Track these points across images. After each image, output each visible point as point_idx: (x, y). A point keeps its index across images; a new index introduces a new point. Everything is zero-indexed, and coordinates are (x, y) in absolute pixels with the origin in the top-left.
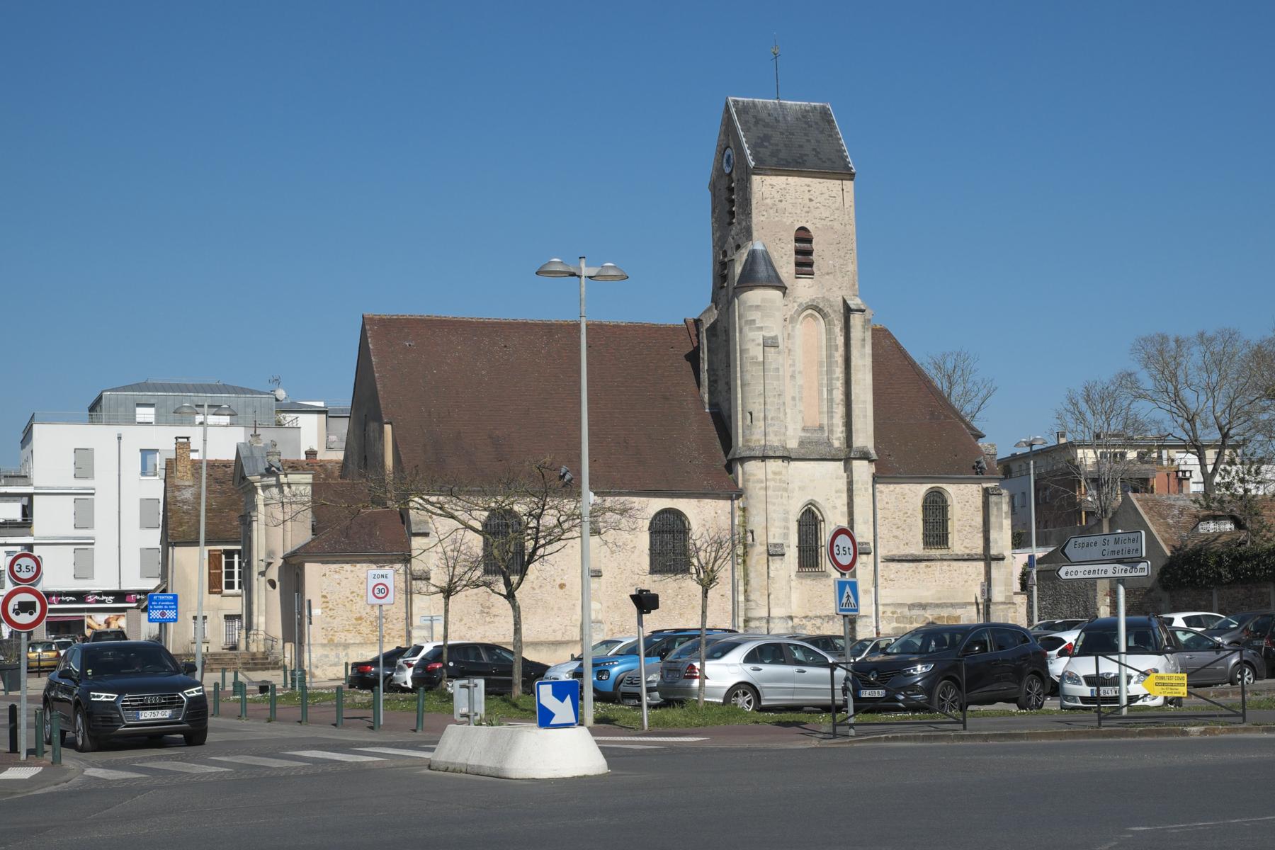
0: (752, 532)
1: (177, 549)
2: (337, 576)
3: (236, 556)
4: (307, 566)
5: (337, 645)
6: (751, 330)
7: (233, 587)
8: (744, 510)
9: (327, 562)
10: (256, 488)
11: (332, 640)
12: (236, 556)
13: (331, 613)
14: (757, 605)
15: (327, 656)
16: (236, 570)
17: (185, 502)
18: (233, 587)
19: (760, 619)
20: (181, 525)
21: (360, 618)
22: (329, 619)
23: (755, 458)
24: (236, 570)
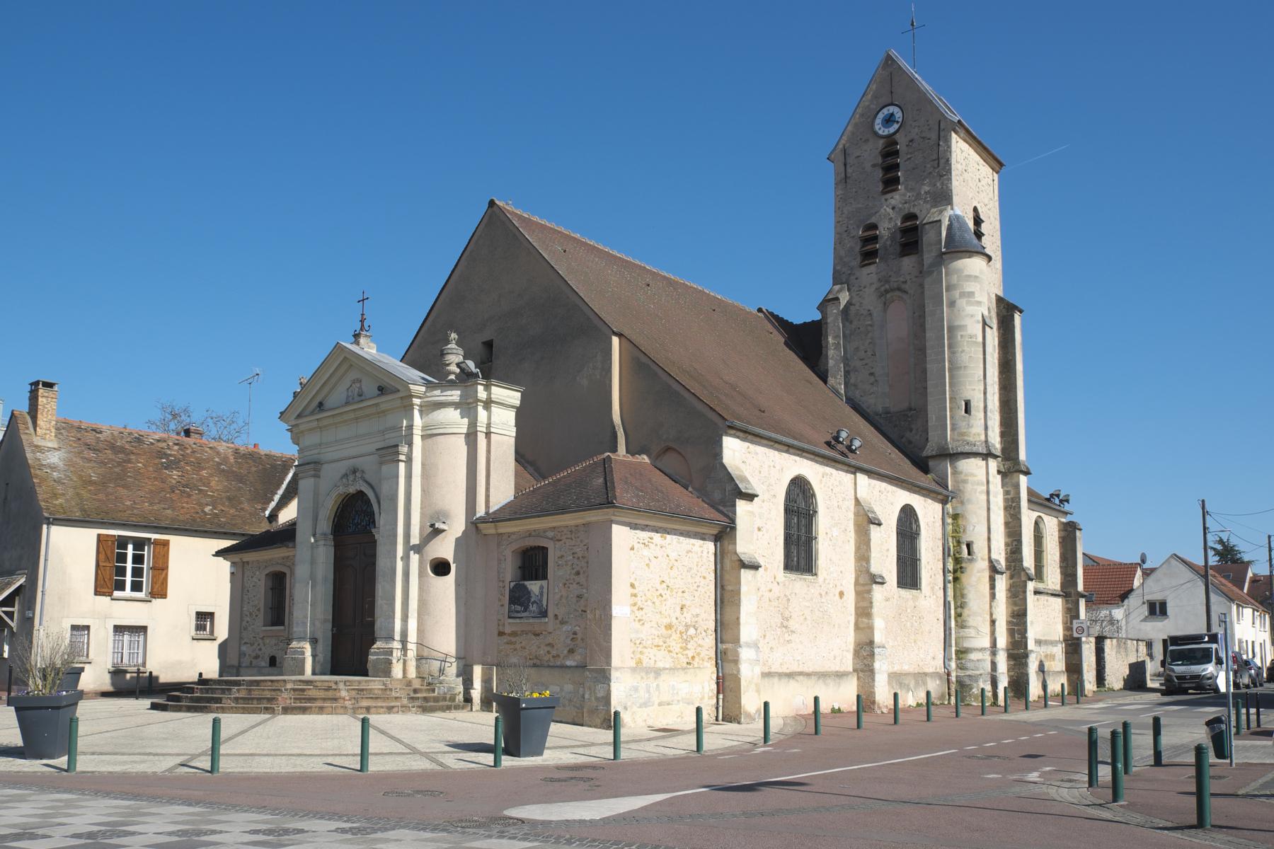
0: (968, 546)
1: (54, 528)
2: (646, 552)
3: (130, 547)
4: (615, 528)
5: (648, 670)
6: (969, 303)
7: (123, 589)
8: (955, 517)
9: (644, 528)
10: (411, 406)
11: (640, 662)
12: (130, 547)
13: (639, 614)
14: (978, 632)
15: (636, 689)
16: (129, 565)
17: (53, 468)
18: (123, 589)
19: (982, 650)
20: (55, 496)
21: (669, 627)
22: (637, 625)
23: (975, 455)
24: (129, 565)
